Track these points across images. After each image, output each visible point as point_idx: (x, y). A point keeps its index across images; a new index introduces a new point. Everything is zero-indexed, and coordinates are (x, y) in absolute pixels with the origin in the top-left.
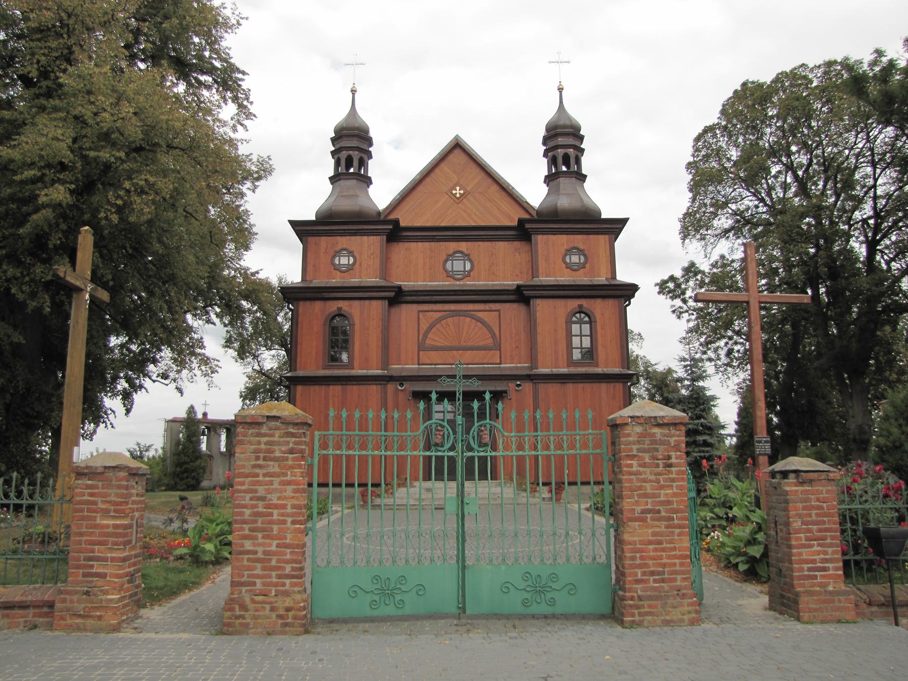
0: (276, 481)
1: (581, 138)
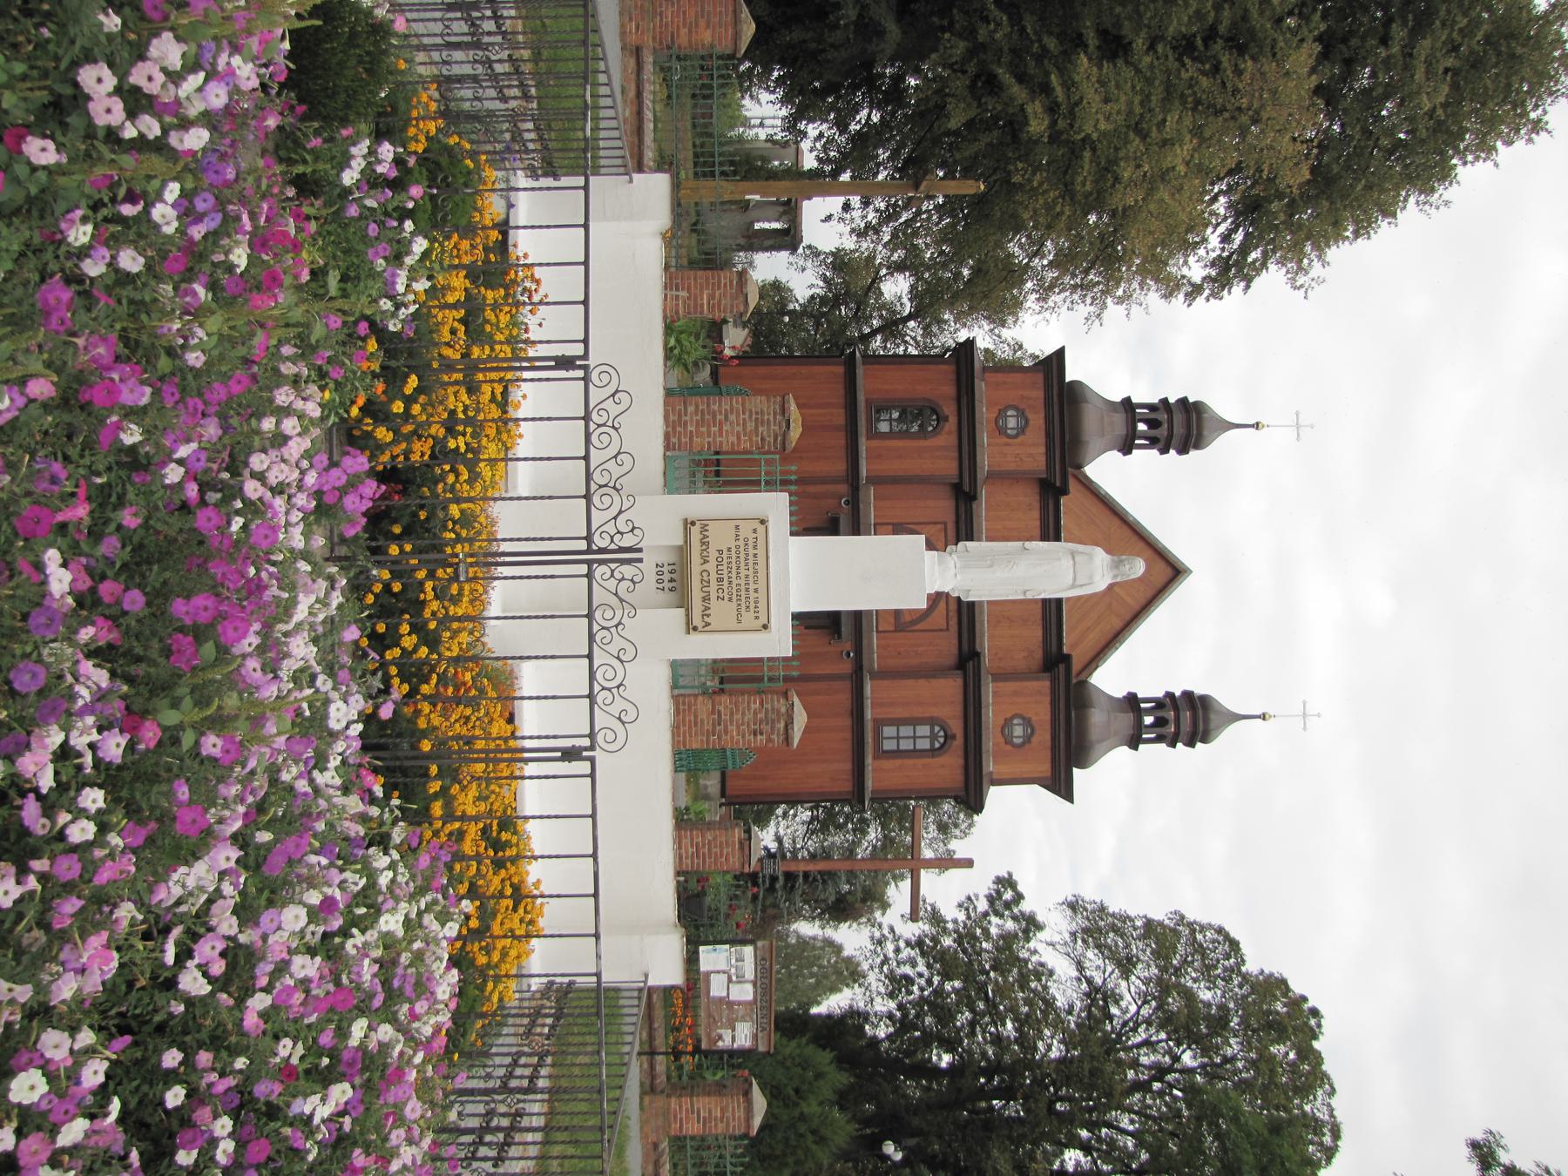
0: (740, 429)
1: (1191, 743)
